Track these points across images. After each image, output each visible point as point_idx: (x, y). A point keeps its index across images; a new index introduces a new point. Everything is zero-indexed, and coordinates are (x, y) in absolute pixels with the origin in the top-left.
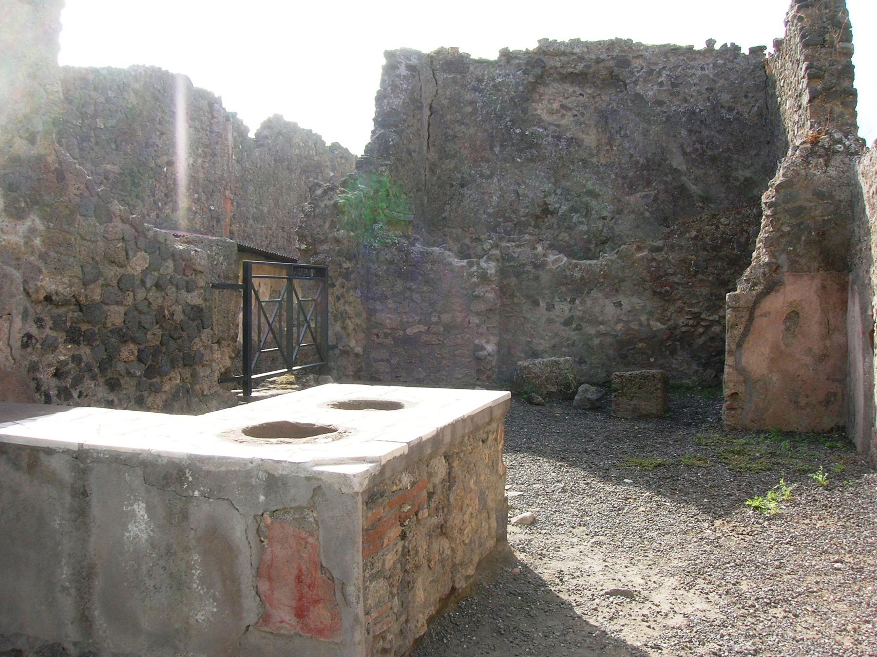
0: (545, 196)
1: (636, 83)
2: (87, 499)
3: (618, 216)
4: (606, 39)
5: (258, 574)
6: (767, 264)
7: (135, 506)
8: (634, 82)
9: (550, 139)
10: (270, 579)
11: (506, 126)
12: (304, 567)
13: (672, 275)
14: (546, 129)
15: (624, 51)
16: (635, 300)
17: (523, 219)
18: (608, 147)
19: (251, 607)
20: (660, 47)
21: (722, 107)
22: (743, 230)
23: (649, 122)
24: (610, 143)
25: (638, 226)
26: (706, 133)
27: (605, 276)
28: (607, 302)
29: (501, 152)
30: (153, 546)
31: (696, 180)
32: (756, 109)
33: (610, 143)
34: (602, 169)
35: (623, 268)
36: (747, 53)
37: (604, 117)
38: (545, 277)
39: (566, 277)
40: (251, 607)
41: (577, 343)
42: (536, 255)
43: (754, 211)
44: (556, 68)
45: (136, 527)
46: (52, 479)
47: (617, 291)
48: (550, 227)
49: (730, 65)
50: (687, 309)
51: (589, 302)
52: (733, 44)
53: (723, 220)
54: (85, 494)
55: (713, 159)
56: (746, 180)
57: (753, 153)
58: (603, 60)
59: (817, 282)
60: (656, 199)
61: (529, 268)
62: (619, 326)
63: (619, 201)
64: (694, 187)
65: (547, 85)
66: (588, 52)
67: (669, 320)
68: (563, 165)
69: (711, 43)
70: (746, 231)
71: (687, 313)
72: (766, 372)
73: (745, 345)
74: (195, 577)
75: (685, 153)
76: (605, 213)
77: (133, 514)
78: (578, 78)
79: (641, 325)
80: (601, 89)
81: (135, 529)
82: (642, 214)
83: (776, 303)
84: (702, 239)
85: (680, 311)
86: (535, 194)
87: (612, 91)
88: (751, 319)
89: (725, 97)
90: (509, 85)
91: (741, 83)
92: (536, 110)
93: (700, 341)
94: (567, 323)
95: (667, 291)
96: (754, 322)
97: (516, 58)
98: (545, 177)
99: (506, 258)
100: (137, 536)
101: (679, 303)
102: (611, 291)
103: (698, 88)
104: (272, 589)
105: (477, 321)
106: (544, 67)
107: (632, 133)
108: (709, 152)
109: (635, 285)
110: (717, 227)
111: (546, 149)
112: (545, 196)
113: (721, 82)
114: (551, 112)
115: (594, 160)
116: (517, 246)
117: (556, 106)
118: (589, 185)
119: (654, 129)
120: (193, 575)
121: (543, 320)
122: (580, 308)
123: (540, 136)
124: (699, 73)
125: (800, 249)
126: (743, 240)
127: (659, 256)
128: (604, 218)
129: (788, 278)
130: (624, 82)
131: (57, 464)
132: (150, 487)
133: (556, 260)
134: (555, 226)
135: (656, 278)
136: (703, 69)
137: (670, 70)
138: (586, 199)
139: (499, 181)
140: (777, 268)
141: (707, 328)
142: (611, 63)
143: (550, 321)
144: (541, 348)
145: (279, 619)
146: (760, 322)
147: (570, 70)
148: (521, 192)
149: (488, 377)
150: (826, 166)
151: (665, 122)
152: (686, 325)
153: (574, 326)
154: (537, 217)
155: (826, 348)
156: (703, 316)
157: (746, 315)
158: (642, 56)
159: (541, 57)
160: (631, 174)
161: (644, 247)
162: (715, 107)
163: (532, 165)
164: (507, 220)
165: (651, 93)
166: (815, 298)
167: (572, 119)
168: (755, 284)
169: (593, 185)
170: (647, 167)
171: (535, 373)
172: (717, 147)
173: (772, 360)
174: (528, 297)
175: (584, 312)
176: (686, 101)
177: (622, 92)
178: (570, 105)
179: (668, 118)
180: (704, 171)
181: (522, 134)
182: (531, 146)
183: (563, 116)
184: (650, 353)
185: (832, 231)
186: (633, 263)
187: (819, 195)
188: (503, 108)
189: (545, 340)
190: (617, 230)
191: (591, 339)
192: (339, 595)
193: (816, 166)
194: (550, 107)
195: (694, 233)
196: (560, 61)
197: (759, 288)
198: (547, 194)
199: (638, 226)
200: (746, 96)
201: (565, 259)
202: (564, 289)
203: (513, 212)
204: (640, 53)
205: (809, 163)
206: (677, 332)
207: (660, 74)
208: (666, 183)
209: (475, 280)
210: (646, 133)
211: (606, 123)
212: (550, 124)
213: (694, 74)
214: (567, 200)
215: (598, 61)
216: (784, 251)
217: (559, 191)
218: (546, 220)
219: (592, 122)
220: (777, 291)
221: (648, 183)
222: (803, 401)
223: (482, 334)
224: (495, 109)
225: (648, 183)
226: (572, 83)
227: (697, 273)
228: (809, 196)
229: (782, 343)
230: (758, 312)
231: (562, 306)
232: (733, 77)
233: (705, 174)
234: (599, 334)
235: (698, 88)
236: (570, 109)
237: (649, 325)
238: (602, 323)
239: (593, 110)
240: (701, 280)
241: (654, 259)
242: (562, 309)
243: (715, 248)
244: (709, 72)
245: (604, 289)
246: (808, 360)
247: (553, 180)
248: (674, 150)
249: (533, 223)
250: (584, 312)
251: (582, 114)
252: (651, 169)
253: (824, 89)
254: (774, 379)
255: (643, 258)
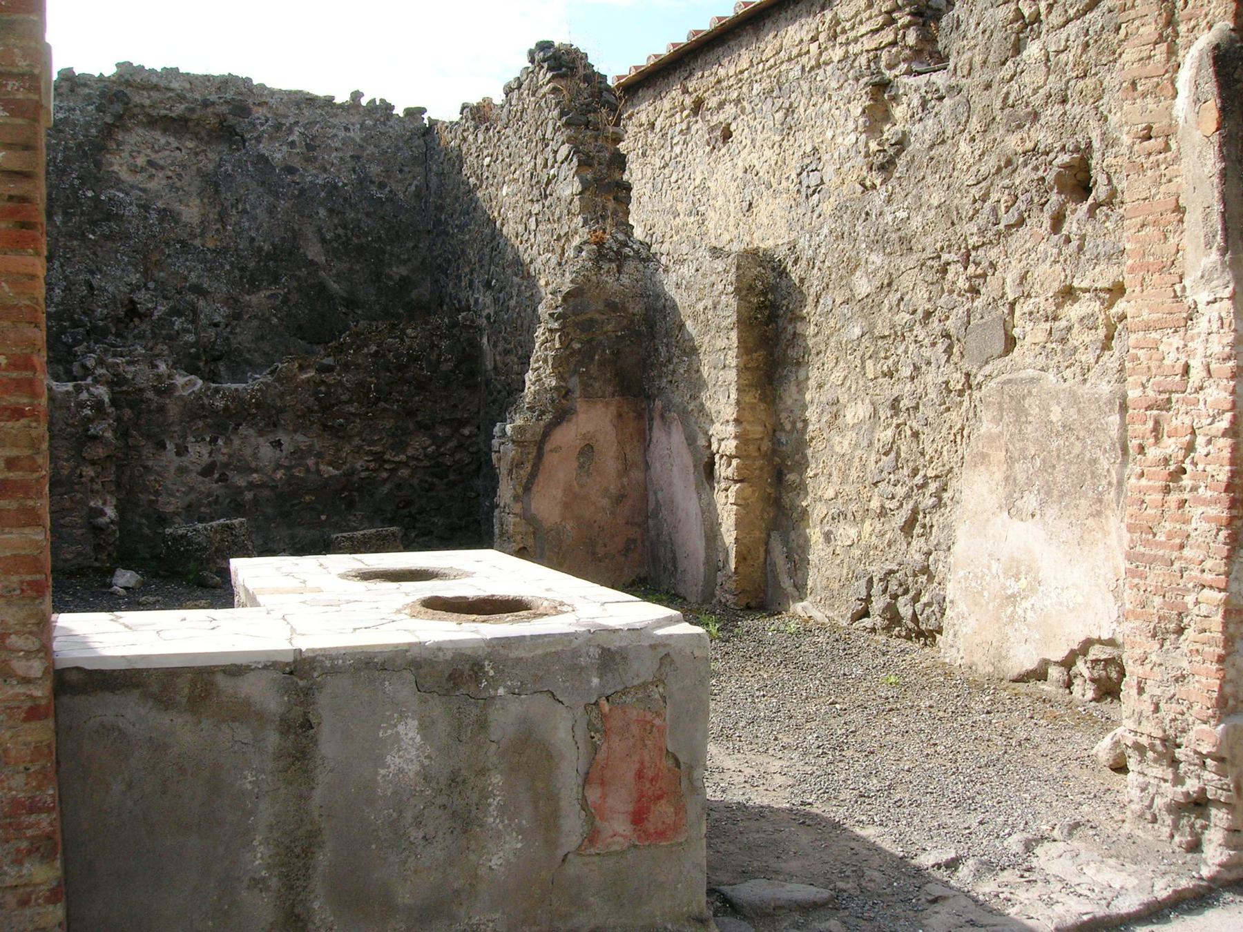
0: (132, 291)
1: (259, 140)
2: (311, 732)
3: (234, 323)
4: (216, 74)
5: (587, 780)
6: (556, 388)
7: (401, 728)
8: (256, 138)
9: (134, 209)
10: (603, 783)
11: (72, 185)
12: (647, 758)
13: (346, 403)
14: (127, 194)
15: (241, 94)
16: (299, 437)
17: (101, 323)
18: (219, 226)
19: (572, 826)
20: (289, 93)
21: (372, 182)
22: (433, 346)
23: (276, 195)
24: (222, 218)
25: (262, 337)
26: (351, 215)
27: (258, 405)
28: (261, 440)
29: (64, 223)
30: (427, 779)
31: (339, 277)
32: (413, 188)
33: (222, 218)
34: (209, 256)
35: (282, 395)
36: (401, 115)
37: (213, 184)
38: (173, 410)
39: (203, 406)
40: (572, 826)
41: (221, 499)
42: (159, 376)
43: (446, 320)
44: (143, 106)
45: (400, 757)
46: (244, 712)
47: (275, 426)
48: (141, 336)
49: (381, 128)
50: (367, 448)
51: (237, 442)
52: (382, 101)
53: (409, 331)
54: (307, 725)
55: (361, 249)
56: (403, 279)
57: (411, 244)
58: (213, 103)
59: (613, 409)
60: (285, 301)
61: (150, 394)
62: (279, 474)
63: (237, 301)
64: (336, 286)
65: (128, 130)
66: (191, 90)
67: (344, 463)
68: (157, 247)
69: (357, 95)
70: (437, 346)
71: (368, 453)
72: (558, 520)
73: (534, 489)
74: (491, 809)
75: (323, 240)
76: (217, 318)
77: (397, 738)
78: (178, 125)
79: (308, 470)
80: (207, 143)
81: (397, 760)
82: (268, 320)
83: (567, 436)
84: (384, 356)
85: (358, 450)
86: (117, 287)
87: (224, 148)
88: (540, 456)
89: (375, 169)
90: (76, 125)
91: (395, 154)
92: (111, 164)
93: (385, 489)
94: (207, 471)
95: (341, 425)
96: (544, 459)
97: (85, 85)
98: (129, 263)
99: (116, 382)
100: (401, 770)
101: (357, 441)
102: (267, 425)
103: (340, 154)
104: (604, 797)
105: (93, 474)
106: (127, 104)
107: (254, 207)
108: (355, 240)
109: (299, 417)
110: (402, 340)
111: (130, 223)
112: (132, 291)
113: (371, 149)
114: (134, 170)
115: (197, 242)
116: (129, 363)
117: (141, 161)
118: (193, 278)
119: (283, 204)
120: (490, 805)
121: (172, 469)
122: (224, 450)
123: (120, 204)
124: (342, 134)
125: (594, 369)
126: (434, 357)
127: (331, 379)
128: (216, 325)
129: (581, 405)
130: (242, 137)
131: (250, 688)
132: (427, 696)
133: (187, 384)
134: (148, 334)
135: (325, 408)
136: (347, 129)
137: (304, 126)
138: (191, 297)
139: (62, 266)
140: (567, 393)
141: (393, 471)
142: (224, 109)
143: (182, 470)
144: (171, 509)
145: (611, 833)
146: (550, 459)
147: (163, 112)
148: (95, 283)
149: (109, 555)
150: (619, 272)
151: (298, 196)
152: (367, 469)
153: (216, 476)
154: (119, 321)
155: (623, 487)
156: (387, 457)
157: (534, 451)
158: (266, 103)
159: (122, 88)
160: (252, 265)
161: (308, 367)
162: (363, 181)
163: (109, 244)
164: (76, 324)
165: (278, 156)
166: (609, 428)
167: (164, 182)
168: (543, 413)
169: (199, 277)
170: (273, 256)
171: (199, 544)
172: (366, 234)
173: (566, 505)
174: (149, 437)
175: (230, 456)
176: (325, 170)
177: (238, 150)
178: (162, 162)
179: (302, 191)
180: (348, 265)
181: (96, 199)
182: (109, 217)
183: (152, 177)
184: (320, 507)
185: (627, 349)
186: (297, 387)
187: (612, 306)
188: (67, 160)
189: (176, 497)
190: (234, 343)
191: (241, 493)
192: (684, 783)
193: (608, 272)
194: (136, 163)
195: (374, 348)
196: (150, 97)
197: (548, 417)
198: (135, 288)
199: (262, 337)
200: (401, 171)
201: (200, 382)
202: (201, 424)
203: (85, 313)
204: (264, 99)
205: (601, 268)
206: (356, 478)
207: (290, 131)
208: (299, 279)
209: (87, 412)
210: (271, 211)
211: (217, 192)
212: (132, 187)
213: (336, 135)
214: (166, 298)
215: (206, 104)
216: (575, 372)
217: (151, 285)
218: (132, 325)
219: (194, 189)
220: (569, 421)
221: (275, 279)
222: (601, 551)
223: (97, 492)
224: (55, 158)
225: (275, 279)
226: (165, 131)
227: (378, 399)
228: (601, 308)
229: (575, 484)
230: (547, 447)
231: (198, 449)
232: (385, 144)
233: (351, 269)
234: (251, 486)
235: (340, 154)
236: (162, 168)
237: (318, 471)
238: (256, 471)
239: (193, 173)
240: (384, 410)
241: (323, 382)
242: (199, 453)
243: (401, 368)
244: (356, 135)
245: (257, 424)
246: (605, 502)
247: (141, 269)
248: (310, 235)
249: (114, 330)
250: (230, 456)
251: (180, 176)
252: (280, 258)
253: (595, 180)
254: (568, 527)
255: (308, 380)
